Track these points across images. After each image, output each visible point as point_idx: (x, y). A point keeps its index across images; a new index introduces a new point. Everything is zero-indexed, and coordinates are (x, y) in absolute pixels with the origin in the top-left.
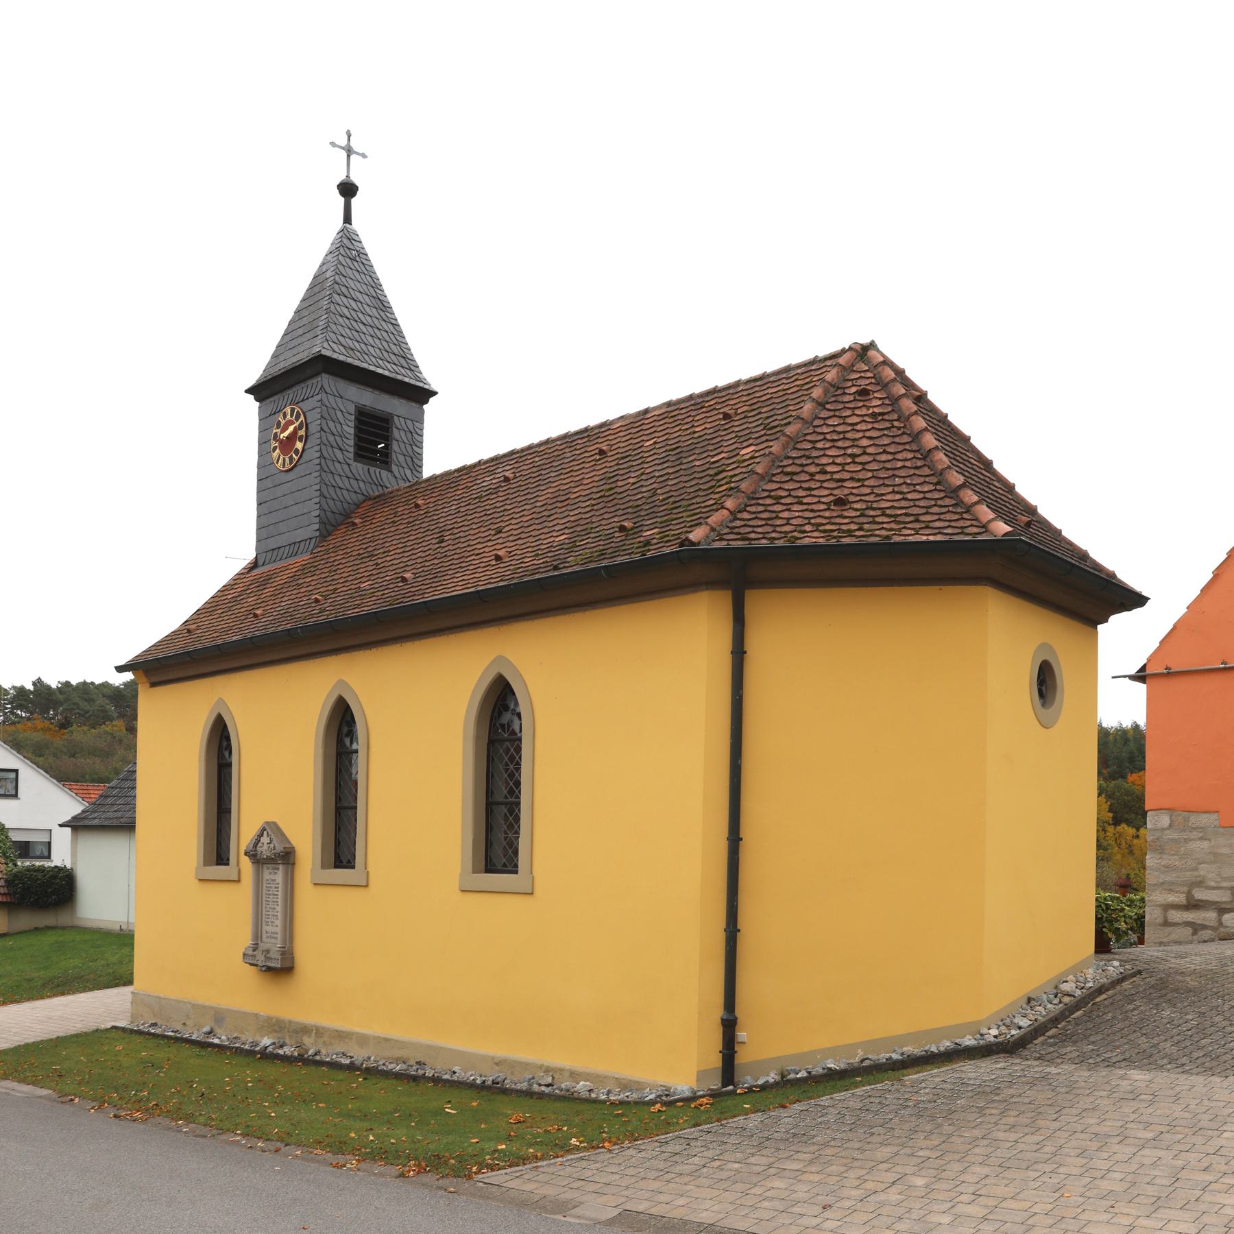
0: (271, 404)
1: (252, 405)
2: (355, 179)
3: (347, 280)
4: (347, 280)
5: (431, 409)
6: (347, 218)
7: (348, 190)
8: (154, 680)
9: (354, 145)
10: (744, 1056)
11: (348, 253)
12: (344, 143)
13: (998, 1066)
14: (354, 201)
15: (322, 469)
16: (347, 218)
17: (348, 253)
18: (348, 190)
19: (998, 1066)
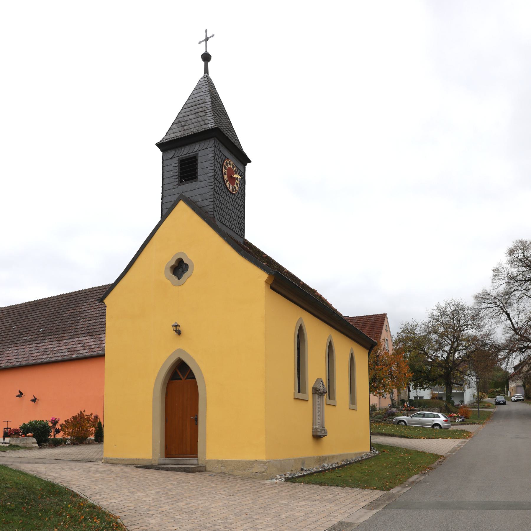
0: (170, 154)
1: (159, 154)
2: (209, 51)
3: (207, 99)
4: (207, 99)
5: (248, 166)
6: (206, 70)
7: (206, 58)
8: (274, 286)
9: (204, 38)
10: (156, 462)
11: (207, 86)
12: (208, 36)
13: (498, 390)
14: (209, 63)
15: (215, 190)
16: (206, 70)
17: (207, 86)
18: (206, 58)
19: (498, 390)
